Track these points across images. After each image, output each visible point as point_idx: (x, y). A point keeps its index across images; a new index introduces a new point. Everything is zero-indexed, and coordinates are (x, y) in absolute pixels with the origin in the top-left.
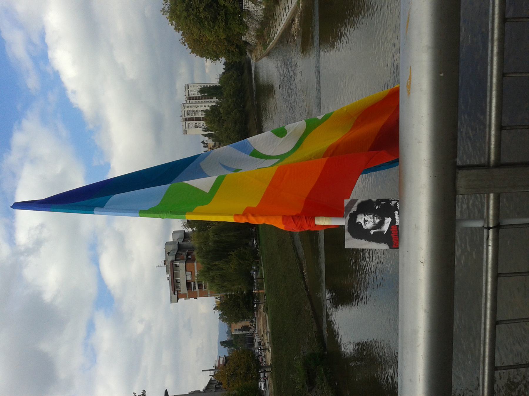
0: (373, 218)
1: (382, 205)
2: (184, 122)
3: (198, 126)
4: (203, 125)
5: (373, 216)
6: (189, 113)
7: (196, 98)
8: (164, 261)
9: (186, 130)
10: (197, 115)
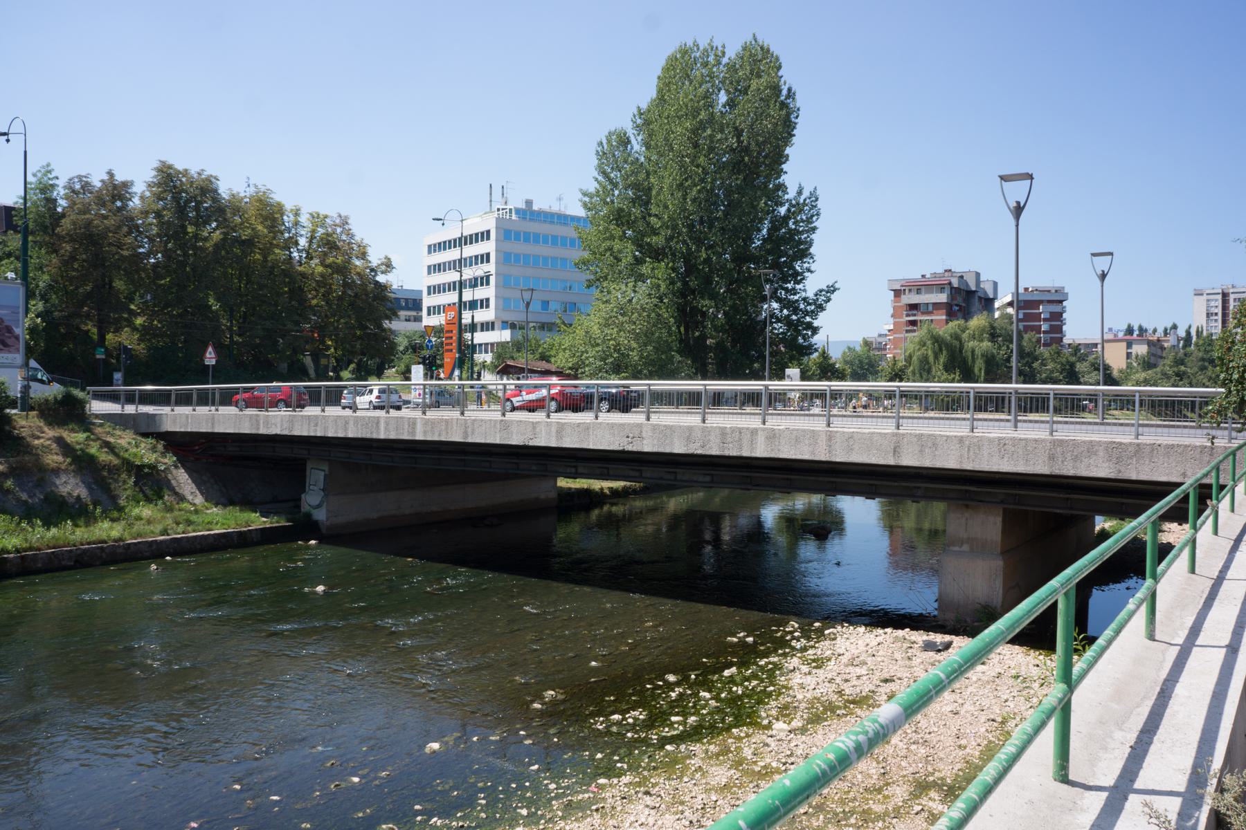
8: (950, 270)
9: (1202, 294)
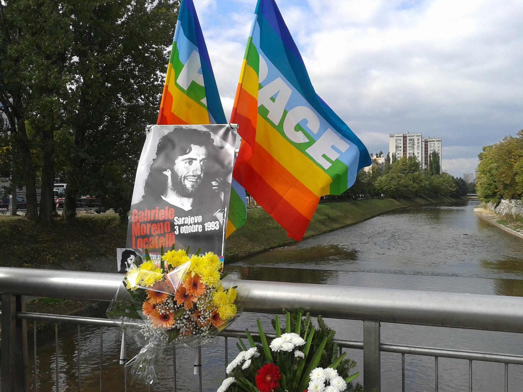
0: (194, 176)
1: (218, 194)
2: (402, 136)
3: (398, 149)
4: (398, 154)
5: (199, 176)
6: (411, 140)
7: (426, 148)
9: (394, 137)
10: (410, 148)
